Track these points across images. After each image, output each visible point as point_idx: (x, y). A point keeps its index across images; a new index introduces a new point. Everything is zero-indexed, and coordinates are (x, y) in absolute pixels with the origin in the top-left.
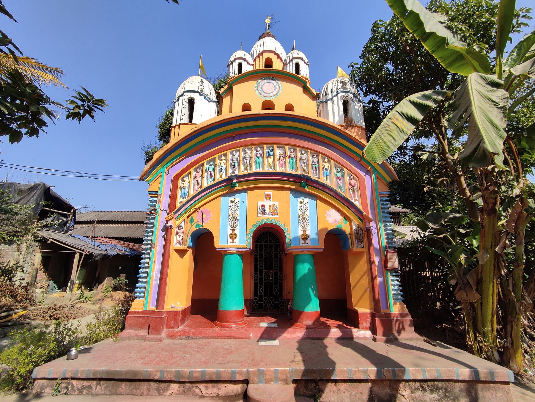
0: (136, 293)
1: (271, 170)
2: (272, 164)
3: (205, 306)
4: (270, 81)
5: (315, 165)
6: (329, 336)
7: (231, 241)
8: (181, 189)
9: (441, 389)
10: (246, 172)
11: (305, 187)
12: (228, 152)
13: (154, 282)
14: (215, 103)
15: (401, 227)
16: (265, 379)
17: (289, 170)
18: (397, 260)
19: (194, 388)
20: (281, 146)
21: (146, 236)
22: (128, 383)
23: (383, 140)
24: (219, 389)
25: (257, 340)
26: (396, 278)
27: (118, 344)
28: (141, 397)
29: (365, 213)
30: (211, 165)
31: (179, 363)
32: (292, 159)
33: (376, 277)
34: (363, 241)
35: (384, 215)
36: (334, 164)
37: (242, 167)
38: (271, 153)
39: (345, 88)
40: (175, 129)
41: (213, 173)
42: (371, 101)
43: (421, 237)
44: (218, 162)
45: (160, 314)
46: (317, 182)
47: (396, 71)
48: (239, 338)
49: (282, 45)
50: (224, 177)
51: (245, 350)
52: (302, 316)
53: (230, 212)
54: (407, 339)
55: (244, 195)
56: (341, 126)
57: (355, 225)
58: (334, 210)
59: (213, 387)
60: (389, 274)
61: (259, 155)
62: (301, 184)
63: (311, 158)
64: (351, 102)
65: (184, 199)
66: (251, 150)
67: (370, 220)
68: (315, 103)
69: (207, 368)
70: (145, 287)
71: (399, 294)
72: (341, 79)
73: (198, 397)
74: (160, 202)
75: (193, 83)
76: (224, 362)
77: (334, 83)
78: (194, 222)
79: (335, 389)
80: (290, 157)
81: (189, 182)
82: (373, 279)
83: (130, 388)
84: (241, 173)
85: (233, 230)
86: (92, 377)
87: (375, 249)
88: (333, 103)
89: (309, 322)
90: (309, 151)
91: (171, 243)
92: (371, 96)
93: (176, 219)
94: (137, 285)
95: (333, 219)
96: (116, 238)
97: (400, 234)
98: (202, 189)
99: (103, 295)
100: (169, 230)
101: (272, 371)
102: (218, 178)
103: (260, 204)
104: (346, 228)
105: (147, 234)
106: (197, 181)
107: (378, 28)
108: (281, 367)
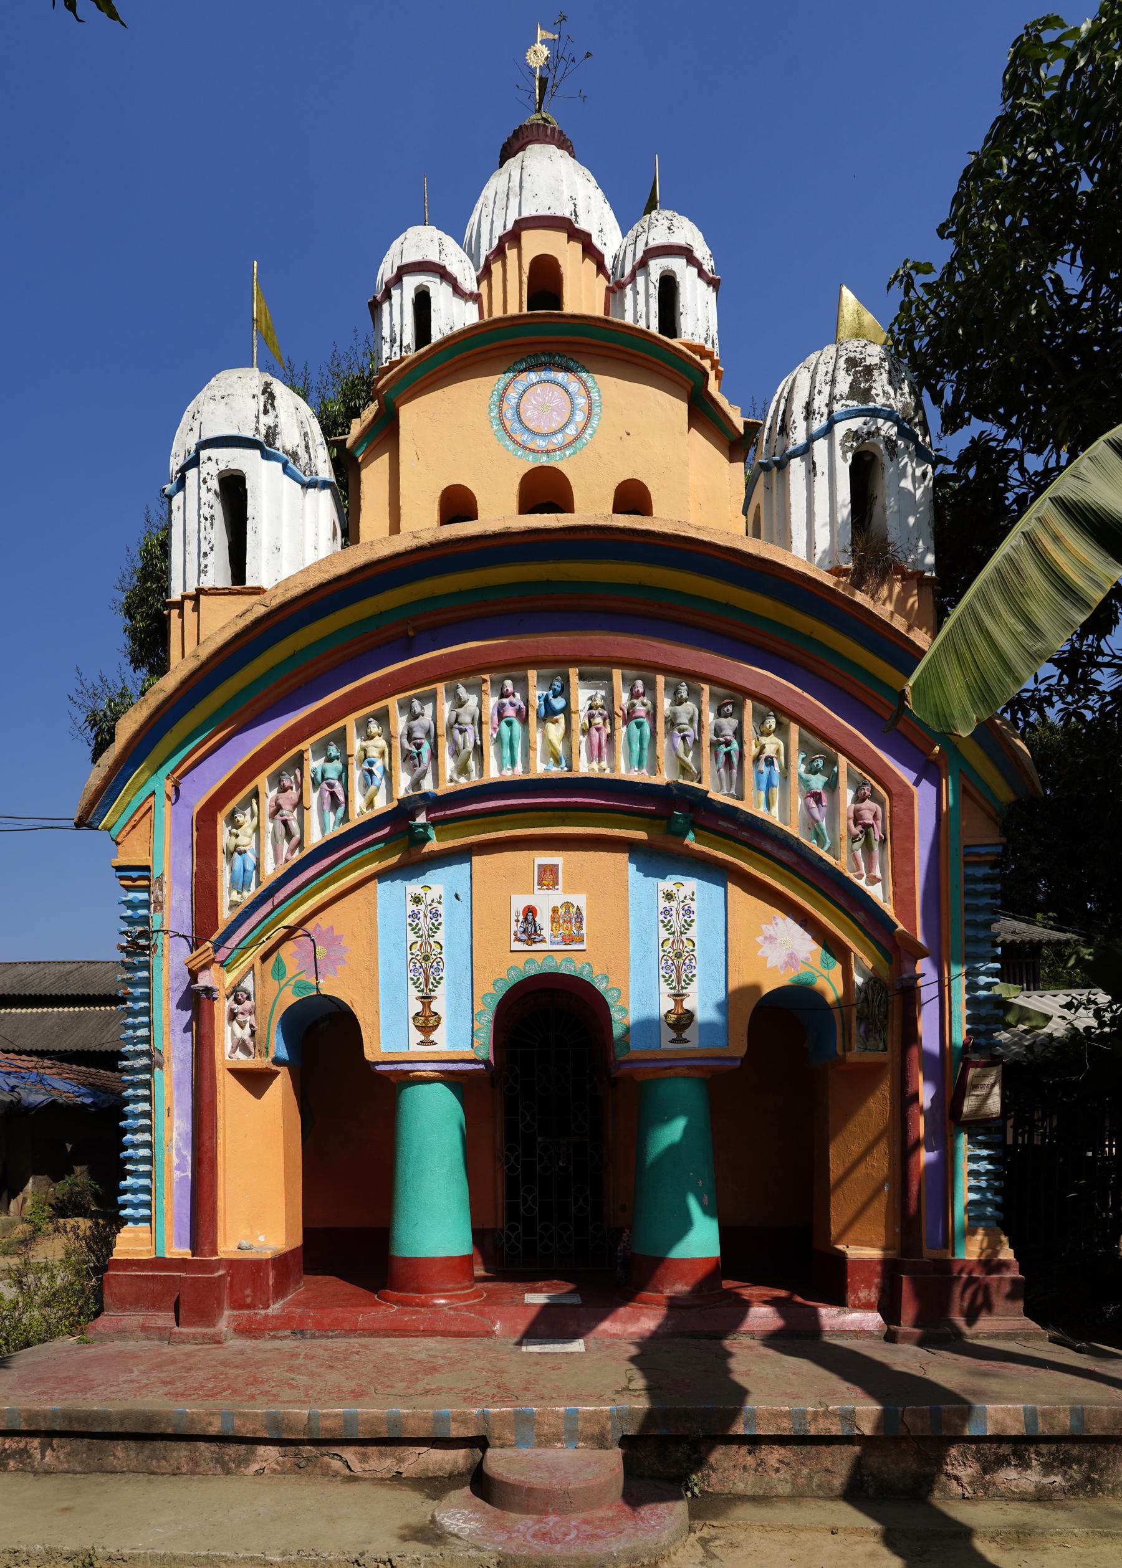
0: (124, 1206)
1: (557, 772)
2: (560, 747)
3: (348, 1237)
5: (728, 743)
6: (745, 1327)
8: (230, 855)
9: (1079, 1461)
10: (463, 782)
12: (392, 703)
13: (177, 1174)
14: (327, 493)
15: (1035, 995)
16: (538, 1436)
17: (624, 769)
18: (997, 1090)
20: (596, 670)
21: (128, 1027)
22: (132, 1444)
24: (401, 1460)
25: (515, 1340)
26: (985, 1152)
27: (90, 1351)
28: (173, 1478)
29: (901, 927)
30: (330, 760)
31: (275, 1395)
32: (639, 725)
33: (917, 1144)
34: (884, 1027)
35: (971, 932)
36: (802, 741)
37: (448, 765)
38: (559, 703)
39: (865, 395)
40: (181, 615)
42: (978, 450)
43: (1102, 1024)
44: (356, 744)
46: (730, 813)
47: (1097, 292)
48: (458, 1335)
49: (601, 184)
50: (381, 804)
51: (479, 1363)
52: (660, 1272)
54: (996, 1336)
55: (460, 871)
57: (863, 973)
58: (790, 921)
59: (381, 1455)
60: (963, 1138)
61: (510, 712)
62: (671, 827)
63: (710, 717)
64: (886, 459)
65: (246, 894)
66: (480, 693)
67: (918, 953)
68: (738, 470)
69: (359, 1406)
70: (147, 1190)
71: (988, 1203)
72: (853, 347)
73: (339, 1478)
74: (159, 905)
75: (231, 400)
76: (411, 1391)
77: (822, 369)
78: (289, 975)
80: (630, 716)
81: (257, 829)
82: (906, 1150)
83: (140, 1457)
84: (446, 787)
85: (426, 1000)
86: (24, 1427)
87: (926, 1056)
88: (812, 470)
89: (681, 1288)
90: (706, 688)
91: (217, 1050)
92: (976, 427)
93: (222, 964)
94: (124, 1184)
95: (783, 951)
96: (42, 1054)
97: (1024, 1014)
99: (28, 1228)
100: (205, 1004)
102: (359, 810)
103: (519, 903)
105: (130, 1020)
106: (285, 823)
108: (585, 1400)
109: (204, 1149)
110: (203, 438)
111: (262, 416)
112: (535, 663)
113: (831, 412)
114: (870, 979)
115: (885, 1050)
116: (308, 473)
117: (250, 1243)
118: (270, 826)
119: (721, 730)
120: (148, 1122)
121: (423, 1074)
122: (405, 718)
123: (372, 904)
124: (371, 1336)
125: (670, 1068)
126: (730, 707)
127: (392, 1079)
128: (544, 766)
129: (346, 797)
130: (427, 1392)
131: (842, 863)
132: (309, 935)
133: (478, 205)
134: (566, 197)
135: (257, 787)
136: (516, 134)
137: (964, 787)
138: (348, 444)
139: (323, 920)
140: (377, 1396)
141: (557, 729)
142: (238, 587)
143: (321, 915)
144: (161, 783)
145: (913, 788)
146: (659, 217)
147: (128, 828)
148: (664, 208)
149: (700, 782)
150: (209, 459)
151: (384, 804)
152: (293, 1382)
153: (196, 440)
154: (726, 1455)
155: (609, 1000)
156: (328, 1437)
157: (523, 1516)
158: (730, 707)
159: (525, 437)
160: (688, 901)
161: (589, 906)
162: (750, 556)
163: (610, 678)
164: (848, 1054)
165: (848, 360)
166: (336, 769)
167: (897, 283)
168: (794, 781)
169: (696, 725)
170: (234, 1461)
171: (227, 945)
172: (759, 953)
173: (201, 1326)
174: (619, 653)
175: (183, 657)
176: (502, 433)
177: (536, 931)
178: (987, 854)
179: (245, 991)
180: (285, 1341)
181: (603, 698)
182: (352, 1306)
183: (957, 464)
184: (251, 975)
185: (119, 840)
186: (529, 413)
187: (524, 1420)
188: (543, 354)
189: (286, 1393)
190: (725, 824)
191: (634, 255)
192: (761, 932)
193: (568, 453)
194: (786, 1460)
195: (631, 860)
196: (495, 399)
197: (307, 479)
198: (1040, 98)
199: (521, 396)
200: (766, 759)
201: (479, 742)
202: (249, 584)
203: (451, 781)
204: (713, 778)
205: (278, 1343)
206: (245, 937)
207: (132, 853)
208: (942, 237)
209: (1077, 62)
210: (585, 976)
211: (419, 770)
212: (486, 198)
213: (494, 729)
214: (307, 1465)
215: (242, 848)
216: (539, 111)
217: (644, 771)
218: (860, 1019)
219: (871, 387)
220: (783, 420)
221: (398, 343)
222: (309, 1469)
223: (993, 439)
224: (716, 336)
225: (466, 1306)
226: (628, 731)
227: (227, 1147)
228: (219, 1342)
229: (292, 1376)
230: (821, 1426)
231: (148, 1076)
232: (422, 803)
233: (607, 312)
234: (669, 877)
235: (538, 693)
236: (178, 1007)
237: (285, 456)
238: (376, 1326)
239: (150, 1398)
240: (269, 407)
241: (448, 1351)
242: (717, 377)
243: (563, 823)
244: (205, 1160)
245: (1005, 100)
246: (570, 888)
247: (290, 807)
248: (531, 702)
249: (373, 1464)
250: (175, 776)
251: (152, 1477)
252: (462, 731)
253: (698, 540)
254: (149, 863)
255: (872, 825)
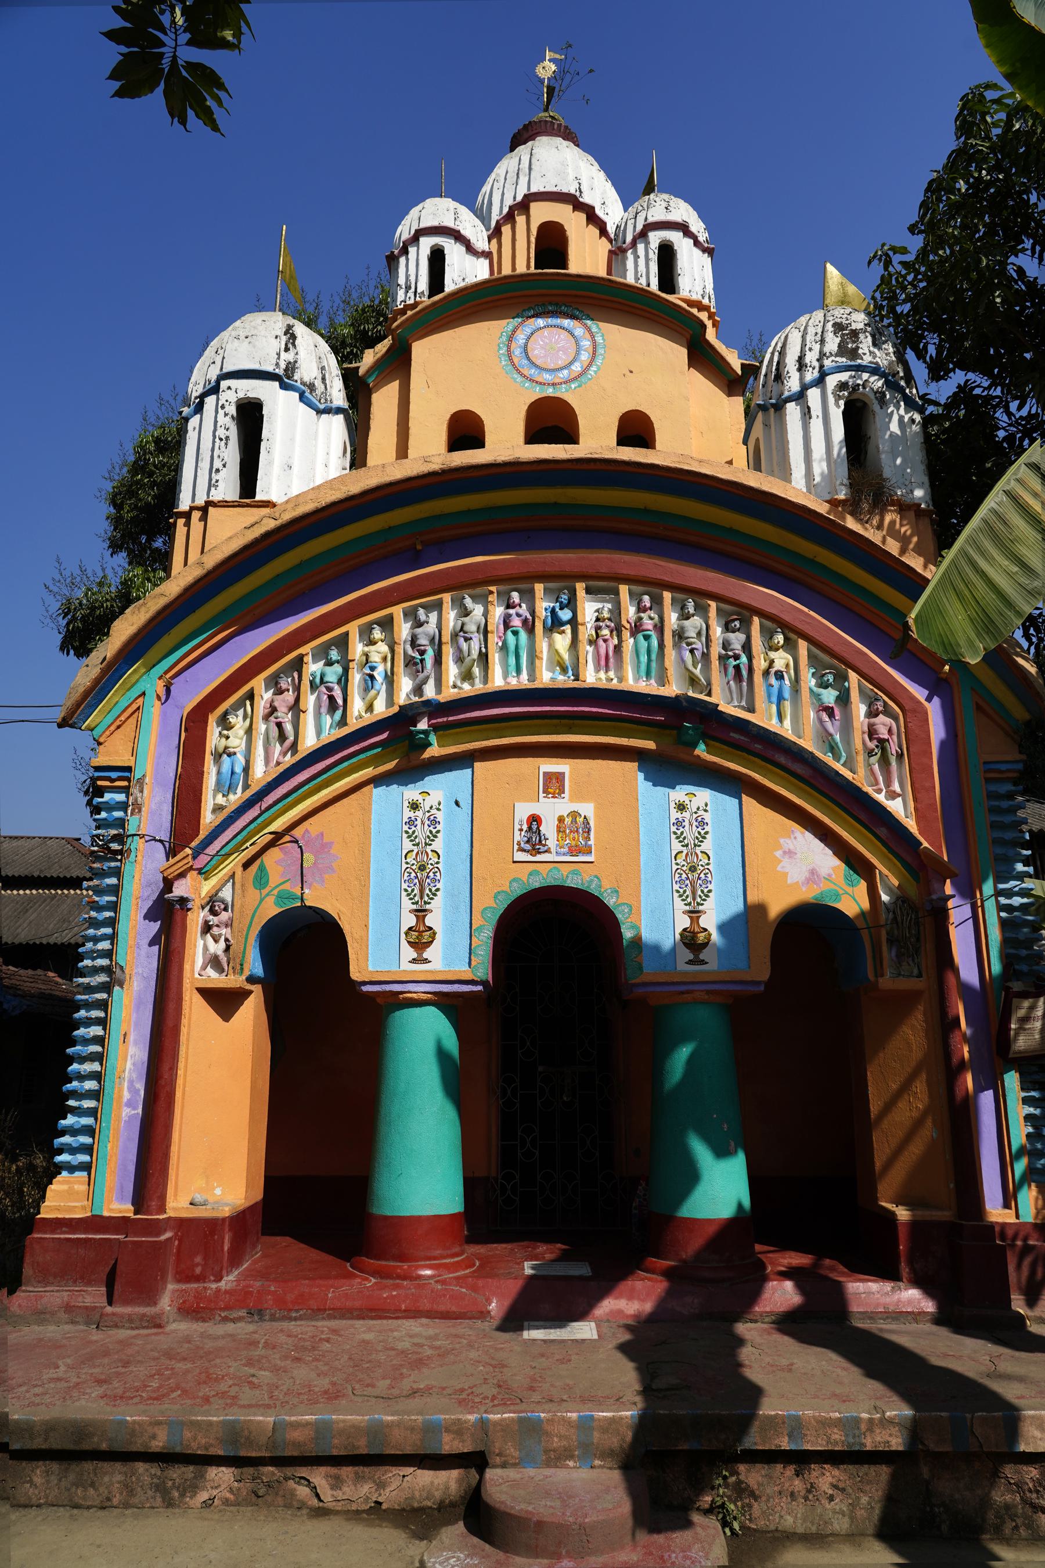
0: (60, 1151)
1: (564, 681)
2: (566, 656)
3: (318, 1195)
4: (558, 321)
5: (737, 657)
7: (410, 953)
11: (695, 745)
12: (397, 611)
13: (126, 1112)
16: (546, 1451)
17: (632, 680)
19: (291, 1483)
20: (603, 585)
22: (55, 1466)
23: (983, 574)
24: (381, 1485)
28: (101, 1513)
29: (925, 844)
30: (329, 663)
31: (234, 1398)
32: (647, 638)
35: (999, 851)
36: (811, 656)
37: (452, 671)
38: (565, 615)
39: (854, 354)
40: (188, 524)
41: (337, 693)
42: (963, 393)
44: (357, 649)
45: (155, 1227)
46: (742, 725)
48: (446, 1316)
49: (603, 167)
50: (381, 708)
51: (473, 1354)
53: (408, 845)
55: (460, 777)
56: (834, 503)
57: (889, 891)
58: (809, 836)
59: (359, 1479)
61: (516, 622)
62: (679, 739)
63: (717, 631)
64: (876, 407)
66: (486, 605)
67: (943, 872)
68: (737, 405)
69: (335, 1411)
70: (90, 1131)
72: (839, 314)
73: (305, 1511)
74: (138, 808)
75: (256, 338)
76: (395, 1392)
77: (811, 331)
78: (272, 883)
79: (798, 1484)
80: (637, 629)
81: (249, 731)
84: (449, 694)
85: (421, 913)
87: (965, 989)
88: (807, 413)
90: (713, 605)
91: (187, 967)
92: (959, 377)
93: (200, 871)
95: (802, 868)
98: (299, 756)
100: (178, 917)
101: (568, 1422)
103: (523, 811)
104: (853, 900)
105: (91, 932)
106: (279, 725)
107: (984, 115)
108: (601, 1405)
109: (162, 1082)
110: (225, 370)
111: (283, 353)
112: (542, 578)
113: (821, 366)
114: (898, 898)
115: (920, 975)
116: (323, 401)
117: (205, 1197)
118: (263, 727)
119: (730, 644)
120: (99, 1049)
121: (414, 996)
122: (409, 625)
123: (366, 810)
124: (343, 1317)
125: (688, 992)
126: (737, 623)
127: (378, 1000)
128: (550, 675)
129: (345, 701)
130: (414, 1393)
131: (859, 778)
132: (297, 842)
133: (490, 180)
134: (571, 177)
135: (252, 689)
136: (525, 127)
137: (977, 704)
138: (361, 372)
139: (312, 826)
140: (356, 1399)
141: (564, 639)
142: (248, 501)
143: (311, 820)
144: (151, 683)
145: (926, 703)
146: (657, 199)
147: (112, 728)
148: (661, 191)
149: (709, 694)
150: (229, 388)
151: (384, 709)
152: (254, 1379)
153: (218, 372)
154: (769, 1477)
155: (619, 916)
156: (295, 1454)
157: (531, 1561)
158: (737, 623)
159: (532, 372)
160: (701, 812)
161: (597, 816)
162: (751, 488)
163: (617, 593)
164: (881, 980)
165: (835, 325)
166: (335, 673)
167: (876, 261)
168: (805, 695)
169: (704, 639)
170: (178, 1488)
171: (207, 851)
172: (779, 868)
173: (140, 1305)
174: (625, 571)
175: (186, 564)
176: (510, 367)
177: (540, 841)
178: (1009, 771)
179: (223, 901)
180: (239, 1325)
181: (610, 611)
182: (321, 1278)
183: (946, 406)
184: (230, 884)
185: (101, 740)
186: (536, 352)
187: (530, 1429)
188: (551, 304)
189: (247, 1395)
190: (736, 736)
191: (635, 227)
192: (779, 847)
193: (573, 386)
194: (841, 1485)
195: (640, 769)
196: (504, 339)
197: (322, 407)
198: (988, 138)
199: (529, 338)
200: (776, 673)
201: (484, 650)
202: (258, 497)
203: (455, 686)
204: (723, 690)
205: (230, 1327)
206: (227, 843)
207: (114, 753)
208: (913, 234)
209: (1013, 126)
210: (593, 889)
211: (421, 676)
212: (498, 175)
213: (500, 637)
214: (267, 1493)
215: (231, 750)
216: (546, 110)
217: (653, 681)
218: (891, 942)
219: (858, 348)
220: (777, 369)
221: (413, 289)
222: (269, 1498)
223: (979, 386)
224: (712, 292)
225: (457, 1278)
226: (636, 643)
227: (188, 1079)
228: (159, 1326)
229: (252, 1371)
230: (878, 1439)
231: (105, 996)
232: (424, 710)
233: (609, 273)
234: (678, 787)
235: (545, 604)
236: (145, 917)
237: (302, 387)
238: (349, 1304)
239: (83, 1402)
240: (290, 346)
241: (435, 1337)
242: (714, 325)
243: (570, 731)
244: (162, 1096)
245: (958, 138)
246: (577, 797)
247: (285, 710)
248: (537, 613)
249: (348, 1491)
250: (168, 676)
251: (75, 1511)
252: (467, 639)
253: (700, 474)
254: (132, 764)
255: (888, 740)
